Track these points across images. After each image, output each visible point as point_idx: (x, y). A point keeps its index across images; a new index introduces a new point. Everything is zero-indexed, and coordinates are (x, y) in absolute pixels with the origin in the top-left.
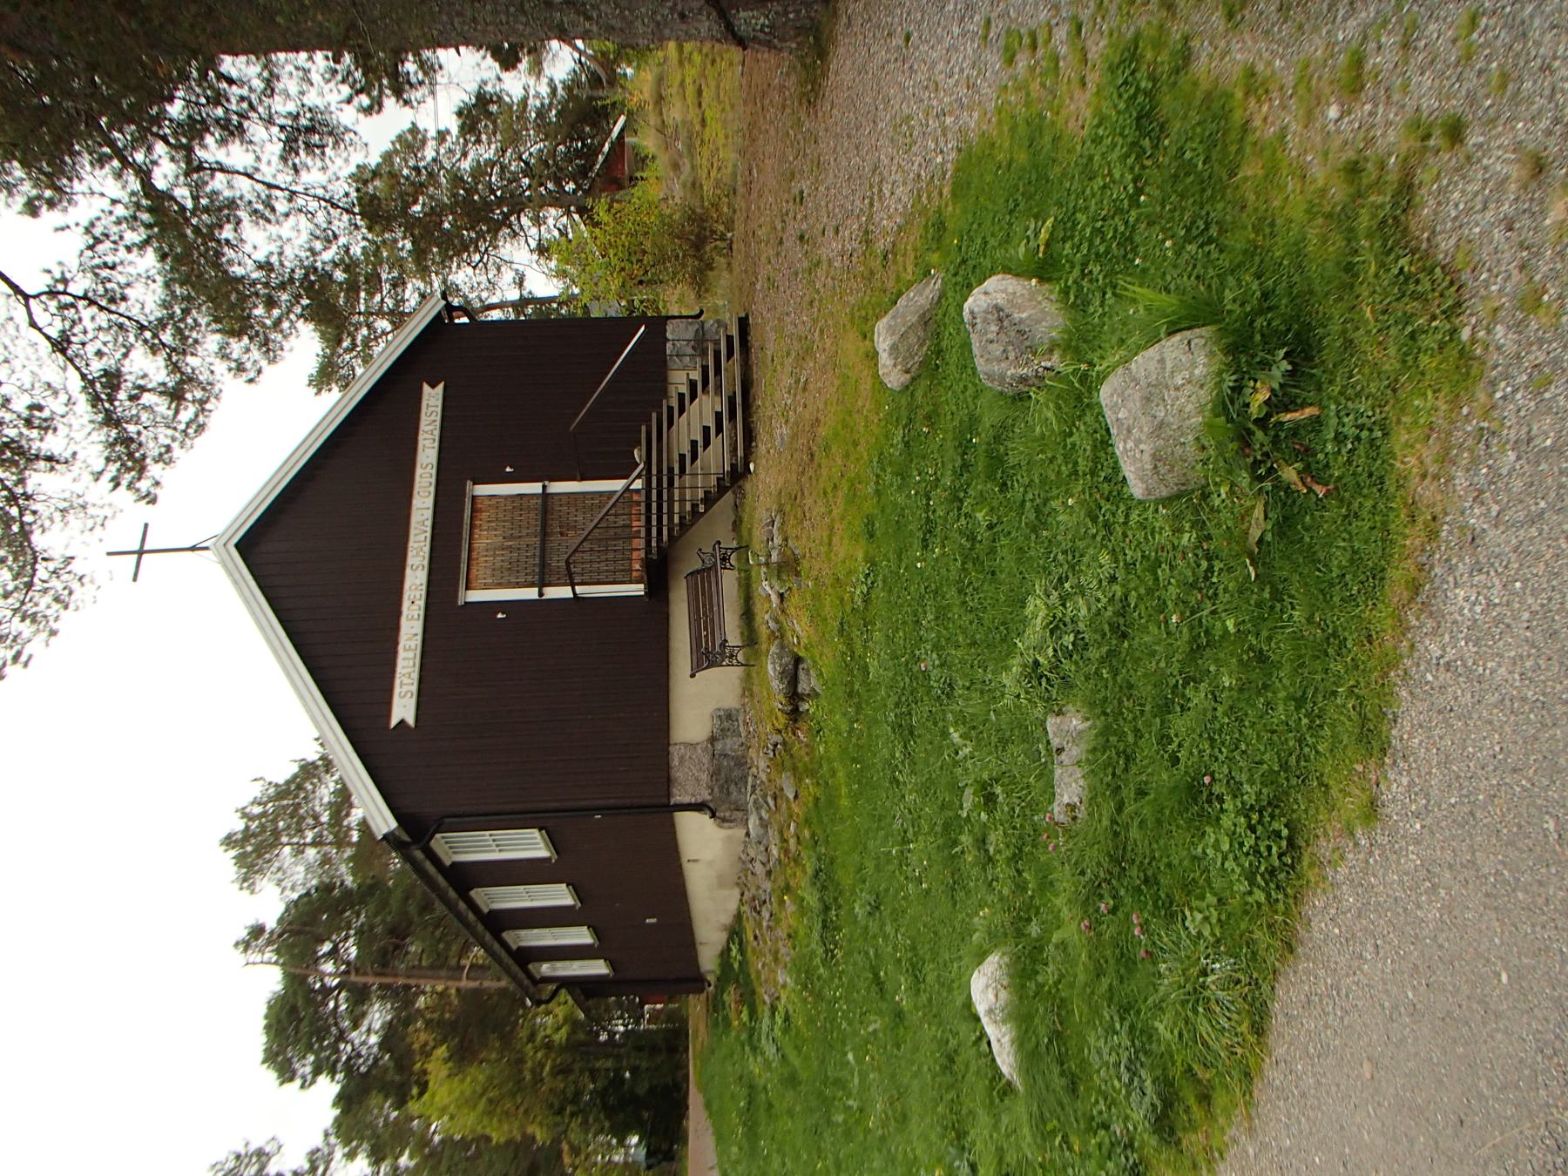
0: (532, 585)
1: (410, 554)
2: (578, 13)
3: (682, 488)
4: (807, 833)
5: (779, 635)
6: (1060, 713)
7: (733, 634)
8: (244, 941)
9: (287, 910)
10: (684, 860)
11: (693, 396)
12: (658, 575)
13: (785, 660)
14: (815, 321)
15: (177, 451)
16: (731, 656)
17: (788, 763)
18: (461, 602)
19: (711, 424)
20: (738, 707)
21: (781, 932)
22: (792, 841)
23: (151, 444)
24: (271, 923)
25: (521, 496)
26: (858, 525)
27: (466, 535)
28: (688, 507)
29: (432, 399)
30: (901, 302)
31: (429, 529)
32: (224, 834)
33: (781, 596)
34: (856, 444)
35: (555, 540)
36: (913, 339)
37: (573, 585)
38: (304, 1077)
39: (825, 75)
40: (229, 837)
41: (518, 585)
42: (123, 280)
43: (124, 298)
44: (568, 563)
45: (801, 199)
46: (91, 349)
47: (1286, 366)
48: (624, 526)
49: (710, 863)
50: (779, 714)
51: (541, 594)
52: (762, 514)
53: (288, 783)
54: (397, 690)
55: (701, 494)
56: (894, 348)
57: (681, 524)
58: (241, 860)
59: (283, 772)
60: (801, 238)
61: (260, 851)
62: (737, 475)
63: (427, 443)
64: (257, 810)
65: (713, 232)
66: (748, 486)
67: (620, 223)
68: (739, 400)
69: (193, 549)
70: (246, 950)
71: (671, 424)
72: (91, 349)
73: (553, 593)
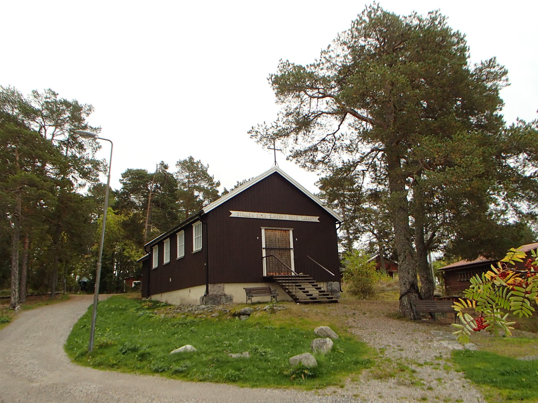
0: (266, 246)
1: (274, 214)
2: (403, 259)
3: (292, 286)
4: (203, 319)
5: (255, 310)
6: (249, 354)
7: (255, 299)
8: (163, 164)
9: (170, 174)
10: (190, 288)
11: (317, 289)
12: (269, 280)
13: (249, 312)
14: (333, 317)
15: (299, 164)
16: (249, 298)
17: (221, 314)
18: (261, 227)
19: (310, 293)
20: (234, 302)
21: (174, 314)
22: (200, 316)
23: (300, 159)
24: (168, 171)
25: (290, 243)
26: (283, 326)
27: (279, 228)
28: (287, 287)
29: (315, 219)
30: (333, 332)
31: (280, 219)
32: (193, 157)
33: (265, 310)
34: (302, 325)
35: (278, 252)
36: (324, 333)
37: (266, 257)
38: (123, 180)
39: (394, 319)
40: (193, 159)
41: (266, 242)
42: (339, 152)
43: (335, 152)
44: (272, 255)
45: (364, 314)
46: (323, 146)
47: (311, 374)
48: (282, 270)
49: (189, 296)
50: (235, 311)
51: (263, 248)
52: (285, 305)
53: (207, 174)
54: (239, 212)
55: (291, 291)
56: (322, 329)
57: (283, 285)
58: (185, 161)
59: (210, 173)
60: (354, 314)
61: (188, 168)
62: (296, 300)
63: (303, 218)
64: (200, 166)
65: (366, 295)
66: (293, 303)
67: (370, 269)
68: (315, 300)
69: (275, 162)
70: (161, 164)
71: (310, 283)
72: (323, 146)
73: (264, 252)
